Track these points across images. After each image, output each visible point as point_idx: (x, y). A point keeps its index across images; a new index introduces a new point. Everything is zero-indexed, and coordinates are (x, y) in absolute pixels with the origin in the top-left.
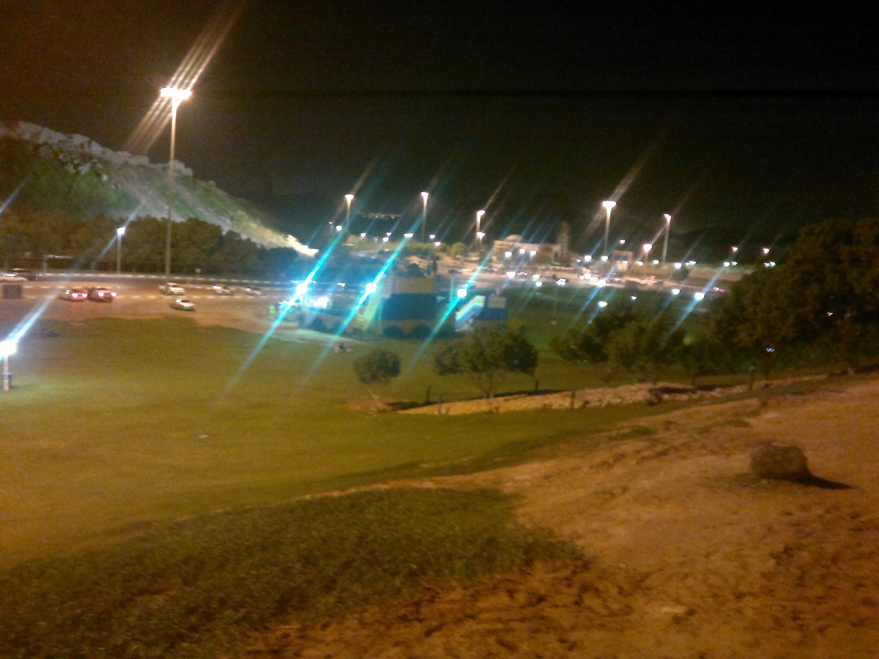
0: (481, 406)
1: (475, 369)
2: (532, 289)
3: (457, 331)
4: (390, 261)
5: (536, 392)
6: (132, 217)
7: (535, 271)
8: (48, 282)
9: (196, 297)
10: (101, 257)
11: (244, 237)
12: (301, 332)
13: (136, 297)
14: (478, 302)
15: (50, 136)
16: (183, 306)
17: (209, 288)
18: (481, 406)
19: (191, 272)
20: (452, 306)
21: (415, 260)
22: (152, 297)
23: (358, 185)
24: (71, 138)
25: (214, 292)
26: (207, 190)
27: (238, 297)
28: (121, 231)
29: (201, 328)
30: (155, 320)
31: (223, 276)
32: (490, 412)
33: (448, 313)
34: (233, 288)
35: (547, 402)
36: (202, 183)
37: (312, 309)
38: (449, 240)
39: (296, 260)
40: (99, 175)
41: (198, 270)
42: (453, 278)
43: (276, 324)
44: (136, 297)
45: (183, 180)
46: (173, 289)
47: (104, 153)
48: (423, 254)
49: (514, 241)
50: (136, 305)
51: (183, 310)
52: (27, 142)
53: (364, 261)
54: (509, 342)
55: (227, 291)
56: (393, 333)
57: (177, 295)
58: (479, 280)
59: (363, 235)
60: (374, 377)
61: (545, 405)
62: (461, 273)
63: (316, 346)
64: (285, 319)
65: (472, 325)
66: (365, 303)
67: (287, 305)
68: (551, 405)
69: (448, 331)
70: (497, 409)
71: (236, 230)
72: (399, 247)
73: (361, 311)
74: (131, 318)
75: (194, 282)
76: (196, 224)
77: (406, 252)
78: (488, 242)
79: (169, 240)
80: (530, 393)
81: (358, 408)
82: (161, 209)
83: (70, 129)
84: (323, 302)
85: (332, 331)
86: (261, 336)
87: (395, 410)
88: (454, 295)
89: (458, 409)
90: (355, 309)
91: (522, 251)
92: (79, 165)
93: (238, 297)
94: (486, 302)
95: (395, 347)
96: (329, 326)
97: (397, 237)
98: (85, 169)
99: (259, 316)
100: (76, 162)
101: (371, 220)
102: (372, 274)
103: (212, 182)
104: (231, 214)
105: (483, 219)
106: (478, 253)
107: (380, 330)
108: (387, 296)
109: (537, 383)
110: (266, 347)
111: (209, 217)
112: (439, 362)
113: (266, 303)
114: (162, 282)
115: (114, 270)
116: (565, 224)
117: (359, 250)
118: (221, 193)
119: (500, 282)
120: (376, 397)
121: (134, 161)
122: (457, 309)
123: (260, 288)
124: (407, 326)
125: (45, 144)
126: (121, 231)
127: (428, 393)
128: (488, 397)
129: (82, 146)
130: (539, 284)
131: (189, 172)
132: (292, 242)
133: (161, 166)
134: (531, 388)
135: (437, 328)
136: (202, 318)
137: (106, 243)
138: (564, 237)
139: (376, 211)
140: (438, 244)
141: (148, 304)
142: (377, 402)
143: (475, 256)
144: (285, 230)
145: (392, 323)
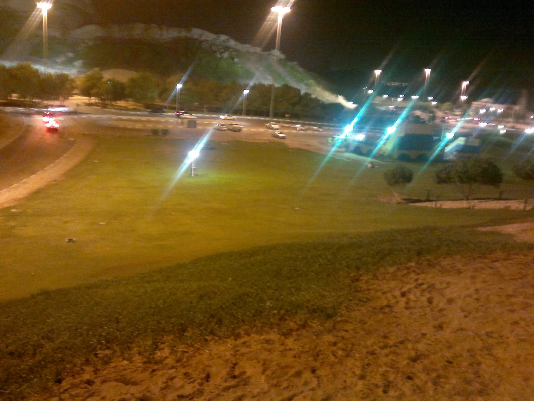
0: (464, 204)
1: (462, 181)
2: (497, 134)
3: (445, 159)
4: (404, 114)
5: (500, 199)
6: (251, 84)
7: (500, 123)
8: (216, 120)
9: (286, 131)
10: (235, 108)
11: (313, 96)
12: (348, 155)
13: (253, 130)
14: (461, 141)
15: (209, 36)
16: (279, 136)
17: (293, 126)
18: (464, 204)
19: (283, 116)
20: (443, 144)
21: (418, 113)
22: (262, 130)
23: (385, 63)
24: (219, 37)
25: (295, 129)
26: (292, 67)
27: (309, 132)
28: (246, 92)
29: (290, 149)
30: (265, 143)
31: (301, 120)
32: (469, 208)
33: (439, 148)
34: (307, 127)
35: (508, 205)
36: (290, 63)
37: (354, 141)
38: (442, 100)
39: (344, 110)
40: (233, 59)
41: (287, 116)
42: (444, 125)
43: (334, 149)
44: (253, 130)
45: (280, 61)
46: (273, 126)
47: (235, 45)
48: (424, 109)
49: (487, 102)
50: (254, 134)
51: (279, 138)
52: (196, 39)
53: (386, 112)
54: (485, 166)
55: (303, 128)
56: (403, 158)
57: (275, 129)
58: (463, 128)
59: (385, 96)
60: (396, 182)
61: (506, 206)
62: (448, 122)
63: (356, 164)
64: (340, 147)
65: (455, 156)
66: (388, 139)
67: (340, 138)
68: (510, 207)
69: (440, 158)
70: (473, 206)
71: (309, 92)
72: (410, 105)
73: (385, 144)
74: (251, 141)
75: (284, 122)
76: (287, 88)
77: (414, 108)
78: (468, 102)
79: (272, 97)
80: (496, 199)
81: (385, 200)
82: (266, 79)
83: (218, 32)
84: (361, 137)
85: (367, 155)
86: (325, 156)
87: (408, 203)
88: (444, 137)
89: (448, 205)
90: (381, 143)
91: (492, 109)
92: (222, 53)
93: (309, 132)
94: (466, 141)
95: (409, 166)
96: (364, 151)
97: (407, 98)
98: (226, 55)
99: (322, 144)
100: (221, 50)
101: (390, 87)
102: (392, 121)
103: (295, 63)
104: (305, 82)
105: (468, 87)
106: (460, 110)
107: (396, 156)
108: (402, 135)
109: (501, 194)
110: (328, 162)
111: (294, 84)
112: (438, 177)
113: (327, 137)
114: (267, 122)
115: (241, 114)
116: (524, 91)
117: (381, 105)
118: (301, 70)
119: (473, 129)
120: (396, 194)
121: (253, 49)
122: (446, 145)
123: (322, 127)
124: (413, 154)
125: (206, 41)
126: (246, 92)
127: (428, 196)
128: (468, 199)
129: (224, 41)
130: (502, 132)
131: (283, 56)
132: (341, 100)
133: (267, 53)
134: (497, 196)
135: (432, 158)
136: (291, 143)
137: (237, 99)
138: (523, 101)
139: (394, 81)
140: (434, 103)
141: (261, 134)
142: (397, 198)
143: (459, 112)
144: (337, 92)
145: (405, 152)
